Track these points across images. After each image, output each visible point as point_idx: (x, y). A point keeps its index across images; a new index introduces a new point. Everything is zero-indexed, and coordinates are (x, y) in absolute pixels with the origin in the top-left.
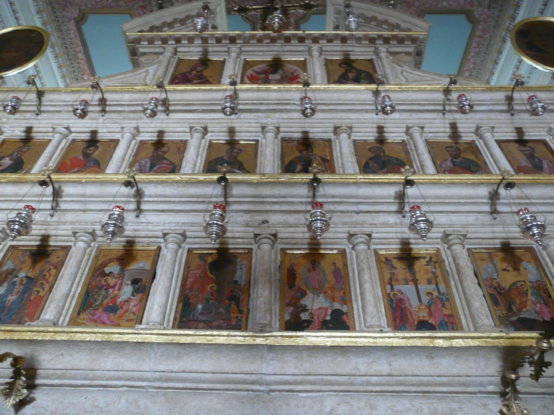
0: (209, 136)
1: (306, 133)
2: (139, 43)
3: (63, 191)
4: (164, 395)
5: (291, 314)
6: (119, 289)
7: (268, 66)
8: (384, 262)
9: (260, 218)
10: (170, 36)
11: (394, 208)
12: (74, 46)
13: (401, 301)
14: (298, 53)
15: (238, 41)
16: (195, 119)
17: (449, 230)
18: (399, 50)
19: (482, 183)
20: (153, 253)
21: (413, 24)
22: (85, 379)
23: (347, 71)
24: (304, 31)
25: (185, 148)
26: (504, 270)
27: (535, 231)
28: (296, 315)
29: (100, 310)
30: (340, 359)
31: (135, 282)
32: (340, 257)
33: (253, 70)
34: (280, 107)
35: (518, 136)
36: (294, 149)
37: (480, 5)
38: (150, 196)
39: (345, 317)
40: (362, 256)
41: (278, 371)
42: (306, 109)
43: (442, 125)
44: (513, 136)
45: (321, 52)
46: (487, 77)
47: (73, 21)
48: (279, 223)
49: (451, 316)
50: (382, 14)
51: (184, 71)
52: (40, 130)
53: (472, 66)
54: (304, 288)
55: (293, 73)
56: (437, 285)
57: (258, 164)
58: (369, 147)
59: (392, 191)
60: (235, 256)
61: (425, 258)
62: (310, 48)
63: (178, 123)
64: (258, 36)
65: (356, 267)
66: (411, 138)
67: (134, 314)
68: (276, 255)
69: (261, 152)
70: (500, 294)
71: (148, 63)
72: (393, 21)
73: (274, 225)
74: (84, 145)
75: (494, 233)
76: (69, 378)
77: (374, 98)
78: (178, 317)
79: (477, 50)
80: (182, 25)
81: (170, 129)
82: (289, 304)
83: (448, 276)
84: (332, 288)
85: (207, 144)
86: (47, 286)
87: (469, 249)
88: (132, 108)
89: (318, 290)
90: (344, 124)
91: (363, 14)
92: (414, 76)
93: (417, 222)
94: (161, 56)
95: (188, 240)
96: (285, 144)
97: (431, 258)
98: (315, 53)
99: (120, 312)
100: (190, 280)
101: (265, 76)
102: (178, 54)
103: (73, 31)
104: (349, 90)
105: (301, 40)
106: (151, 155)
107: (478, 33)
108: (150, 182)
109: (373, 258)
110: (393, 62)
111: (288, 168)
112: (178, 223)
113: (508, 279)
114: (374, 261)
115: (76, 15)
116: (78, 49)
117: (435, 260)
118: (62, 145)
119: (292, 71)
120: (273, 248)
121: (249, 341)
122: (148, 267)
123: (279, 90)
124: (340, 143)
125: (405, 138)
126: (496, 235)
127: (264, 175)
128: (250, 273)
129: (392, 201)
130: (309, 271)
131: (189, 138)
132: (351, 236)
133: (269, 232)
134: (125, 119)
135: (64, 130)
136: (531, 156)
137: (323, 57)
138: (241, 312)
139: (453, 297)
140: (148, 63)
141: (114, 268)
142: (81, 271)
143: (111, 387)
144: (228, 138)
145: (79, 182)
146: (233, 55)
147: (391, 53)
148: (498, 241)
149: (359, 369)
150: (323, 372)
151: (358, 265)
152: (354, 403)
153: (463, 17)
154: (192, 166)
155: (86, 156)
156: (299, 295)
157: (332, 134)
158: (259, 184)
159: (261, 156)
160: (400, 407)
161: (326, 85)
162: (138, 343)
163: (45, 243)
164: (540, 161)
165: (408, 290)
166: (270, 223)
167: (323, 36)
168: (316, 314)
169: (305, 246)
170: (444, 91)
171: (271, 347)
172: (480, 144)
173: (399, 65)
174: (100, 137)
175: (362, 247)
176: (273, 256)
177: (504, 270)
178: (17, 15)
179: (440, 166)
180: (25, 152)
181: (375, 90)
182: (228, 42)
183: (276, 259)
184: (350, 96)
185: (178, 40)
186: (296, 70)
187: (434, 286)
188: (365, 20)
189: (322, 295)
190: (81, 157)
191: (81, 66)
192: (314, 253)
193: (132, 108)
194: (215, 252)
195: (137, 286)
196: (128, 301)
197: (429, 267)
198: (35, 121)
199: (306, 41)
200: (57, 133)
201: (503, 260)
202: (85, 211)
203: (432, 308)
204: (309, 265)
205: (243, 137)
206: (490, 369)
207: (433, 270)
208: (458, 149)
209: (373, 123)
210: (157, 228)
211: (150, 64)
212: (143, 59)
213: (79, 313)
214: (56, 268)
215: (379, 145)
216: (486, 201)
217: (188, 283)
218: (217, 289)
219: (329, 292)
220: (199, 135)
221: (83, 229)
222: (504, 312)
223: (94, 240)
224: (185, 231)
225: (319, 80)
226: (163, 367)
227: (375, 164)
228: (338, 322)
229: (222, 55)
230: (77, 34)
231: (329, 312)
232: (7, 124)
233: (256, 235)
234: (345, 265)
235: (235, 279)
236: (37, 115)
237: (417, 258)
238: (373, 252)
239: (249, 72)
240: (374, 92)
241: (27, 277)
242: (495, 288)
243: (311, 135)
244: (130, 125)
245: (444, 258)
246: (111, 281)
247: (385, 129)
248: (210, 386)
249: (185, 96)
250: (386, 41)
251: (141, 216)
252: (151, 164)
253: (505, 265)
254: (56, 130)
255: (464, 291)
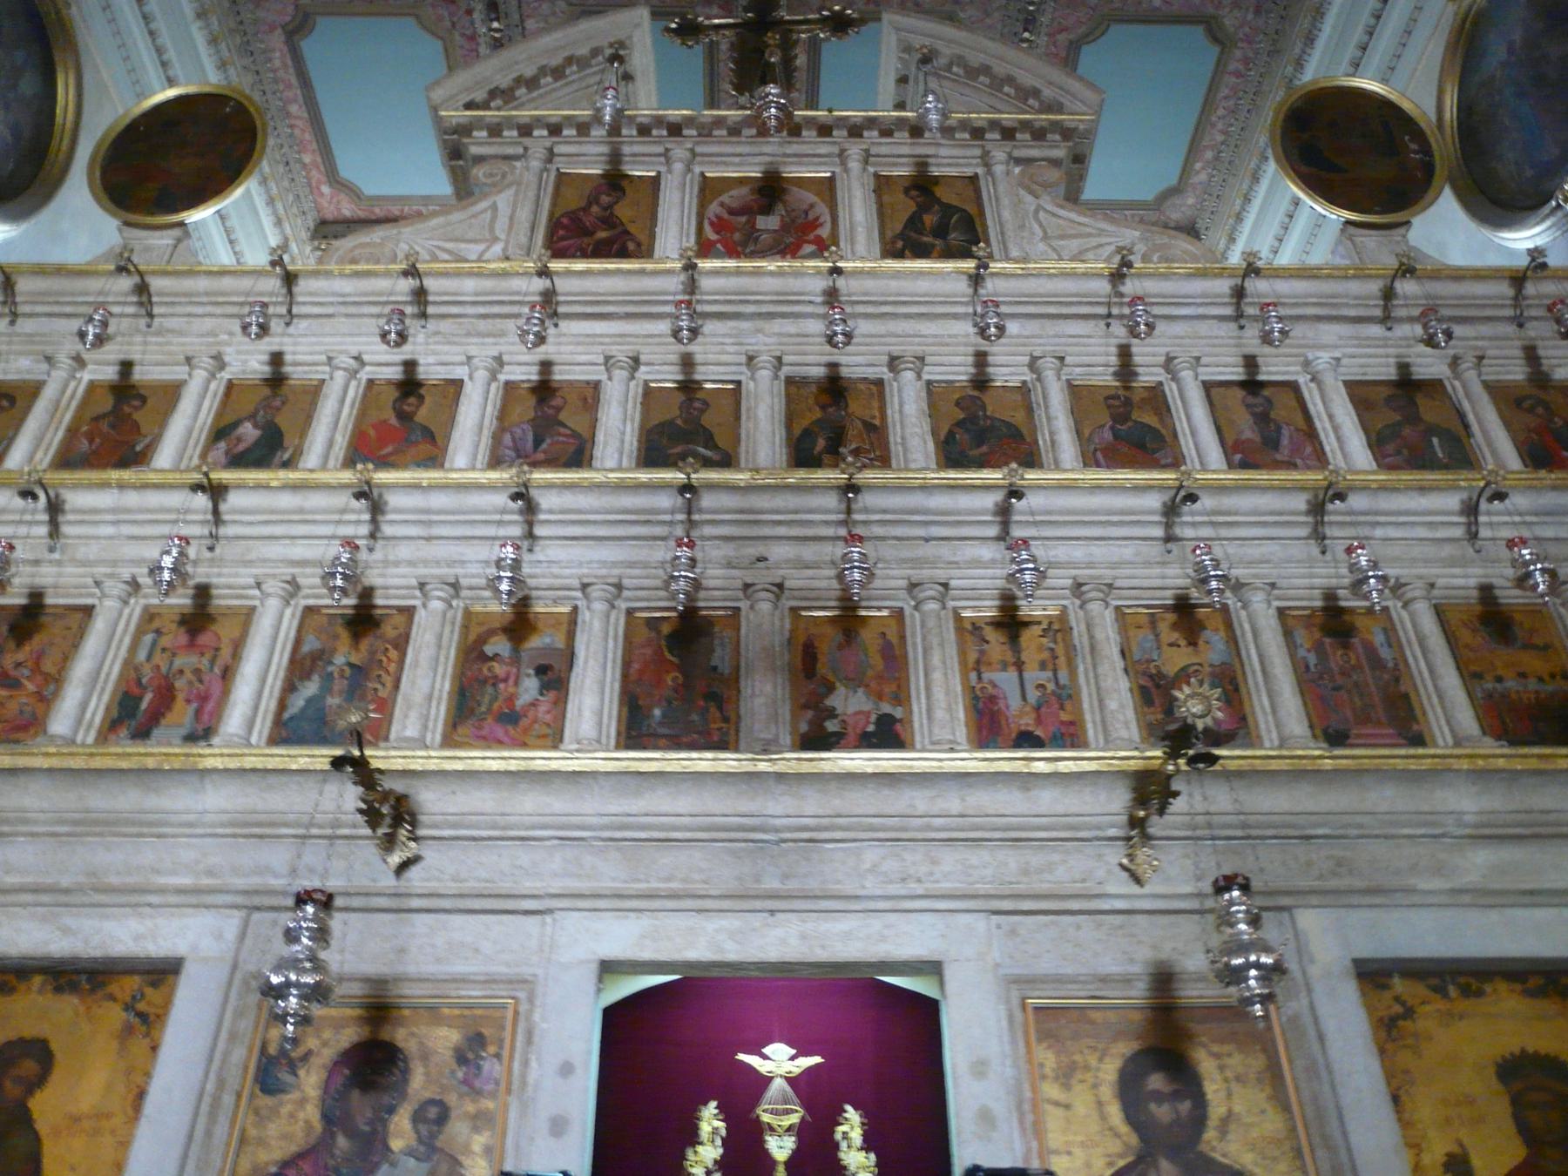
0: (643, 373)
1: (833, 366)
2: (469, 135)
3: (386, 503)
4: (618, 849)
5: (810, 723)
6: (516, 684)
7: (753, 191)
8: (969, 631)
9: (752, 551)
10: (538, 119)
11: (993, 531)
12: (281, 87)
13: (993, 699)
14: (816, 160)
15: (686, 132)
16: (615, 333)
17: (1083, 573)
18: (1034, 153)
19: (1151, 487)
20: (565, 619)
21: (1067, 92)
22: (494, 828)
23: (923, 208)
24: (830, 111)
25: (596, 400)
26: (1171, 645)
27: (1214, 584)
28: (817, 724)
29: (490, 720)
30: (886, 792)
31: (541, 670)
32: (893, 622)
33: (722, 205)
34: (782, 308)
35: (1248, 374)
36: (811, 401)
37: (1236, 5)
38: (551, 512)
39: (898, 727)
40: (931, 623)
41: (791, 811)
42: (835, 334)
43: (1103, 349)
44: (1236, 373)
45: (867, 158)
46: (1252, 165)
47: (279, 31)
48: (787, 561)
49: (1072, 723)
50: (1002, 59)
51: (573, 206)
52: (300, 358)
53: (1220, 138)
54: (831, 677)
55: (806, 213)
56: (1055, 671)
57: (743, 436)
58: (957, 396)
59: (990, 500)
60: (710, 621)
61: (1039, 623)
62: (843, 151)
63: (578, 344)
64: (729, 122)
65: (919, 640)
66: (1039, 379)
67: (548, 725)
68: (782, 620)
69: (748, 410)
70: (1158, 686)
71: (494, 185)
72: (1027, 80)
73: (778, 566)
74: (394, 394)
75: (1164, 577)
76: (468, 827)
77: (970, 291)
78: (623, 729)
79: (1232, 102)
80: (556, 80)
81: (569, 358)
82: (806, 707)
83: (1469, 434)
84: (880, 678)
85: (640, 390)
86: (388, 680)
87: (1117, 608)
88: (482, 310)
89: (856, 681)
90: (909, 349)
91: (960, 57)
92: (1061, 222)
93: (1021, 571)
94: (518, 164)
95: (626, 593)
96: (793, 390)
97: (1050, 623)
98: (854, 165)
99: (524, 722)
100: (636, 666)
101: (748, 222)
102: (557, 159)
103: (278, 54)
104: (921, 274)
105: (825, 130)
106: (532, 414)
107: (1232, 66)
108: (550, 486)
109: (951, 625)
110: (1021, 184)
111: (802, 454)
112: (605, 562)
113: (1175, 659)
114: (952, 630)
115: (288, 19)
116: (289, 94)
117: (1058, 628)
118: (351, 393)
119: (805, 207)
120: (776, 607)
121: (748, 767)
122: (560, 643)
123: (780, 273)
124: (900, 390)
125: (1028, 377)
126: (1169, 582)
127: (757, 471)
128: (738, 653)
129: (989, 518)
130: (840, 647)
131: (604, 377)
132: (913, 586)
133: (770, 580)
134: (468, 334)
135: (352, 361)
136: (1263, 419)
137: (871, 170)
138: (726, 720)
139: (1078, 693)
140: (494, 185)
141: (499, 646)
142: (443, 652)
143: (534, 839)
144: (680, 377)
145: (416, 487)
146: (678, 167)
147: (1019, 161)
148: (1169, 593)
149: (913, 806)
150: (860, 812)
151: (924, 639)
152: (908, 856)
153: (1199, 31)
154: (618, 444)
155: (404, 417)
156: (822, 690)
157: (885, 369)
158: (749, 489)
159: (748, 418)
160: (974, 860)
161: (876, 260)
162: (574, 772)
163: (366, 602)
164: (1279, 429)
165: (1006, 681)
166: (771, 560)
167: (871, 122)
168: (851, 721)
169: (833, 604)
170: (1112, 275)
171: (780, 776)
172: (1171, 390)
173: (1031, 192)
174: (422, 373)
175: (932, 606)
176: (777, 623)
177: (1171, 645)
178: (153, 26)
179: (1089, 439)
180: (278, 409)
181: (973, 271)
182: (665, 133)
183: (782, 627)
184: (923, 285)
185: (555, 130)
186: (812, 206)
187: (1050, 674)
188: (966, 72)
189: (861, 691)
190: (394, 421)
191: (297, 132)
192: (849, 618)
193: (482, 310)
194: (674, 614)
195: (545, 678)
196: (534, 704)
197: (1044, 640)
198: (286, 340)
199: (835, 133)
200: (339, 368)
201: (1175, 626)
202: (429, 539)
203: (1043, 710)
204: (840, 638)
205: (711, 376)
206: (1115, 803)
207: (1052, 645)
208: (1128, 402)
209: (966, 345)
210: (568, 571)
211: (498, 187)
212: (479, 172)
213: (455, 726)
214: (396, 647)
215: (976, 393)
216: (1157, 518)
217: (632, 671)
218: (684, 679)
219: (873, 685)
220: (625, 374)
221: (437, 577)
222: (1160, 716)
223: (457, 596)
224: (620, 578)
225: (861, 248)
226: (613, 809)
227: (966, 437)
228: (888, 735)
229: (653, 163)
230: (290, 63)
231: (873, 718)
232: (229, 345)
233: (747, 586)
234: (903, 638)
235: (713, 663)
236: (288, 324)
237: (1026, 624)
238: (951, 614)
239: (714, 209)
240: (970, 276)
241: (350, 665)
242: (1151, 676)
243: (845, 372)
244: (484, 351)
245: (1074, 624)
246: (499, 669)
247: (990, 359)
248: (688, 835)
249: (588, 284)
250: (1008, 134)
251: (537, 549)
252: (535, 436)
253: (1175, 636)
254: (335, 362)
255: (1097, 683)
